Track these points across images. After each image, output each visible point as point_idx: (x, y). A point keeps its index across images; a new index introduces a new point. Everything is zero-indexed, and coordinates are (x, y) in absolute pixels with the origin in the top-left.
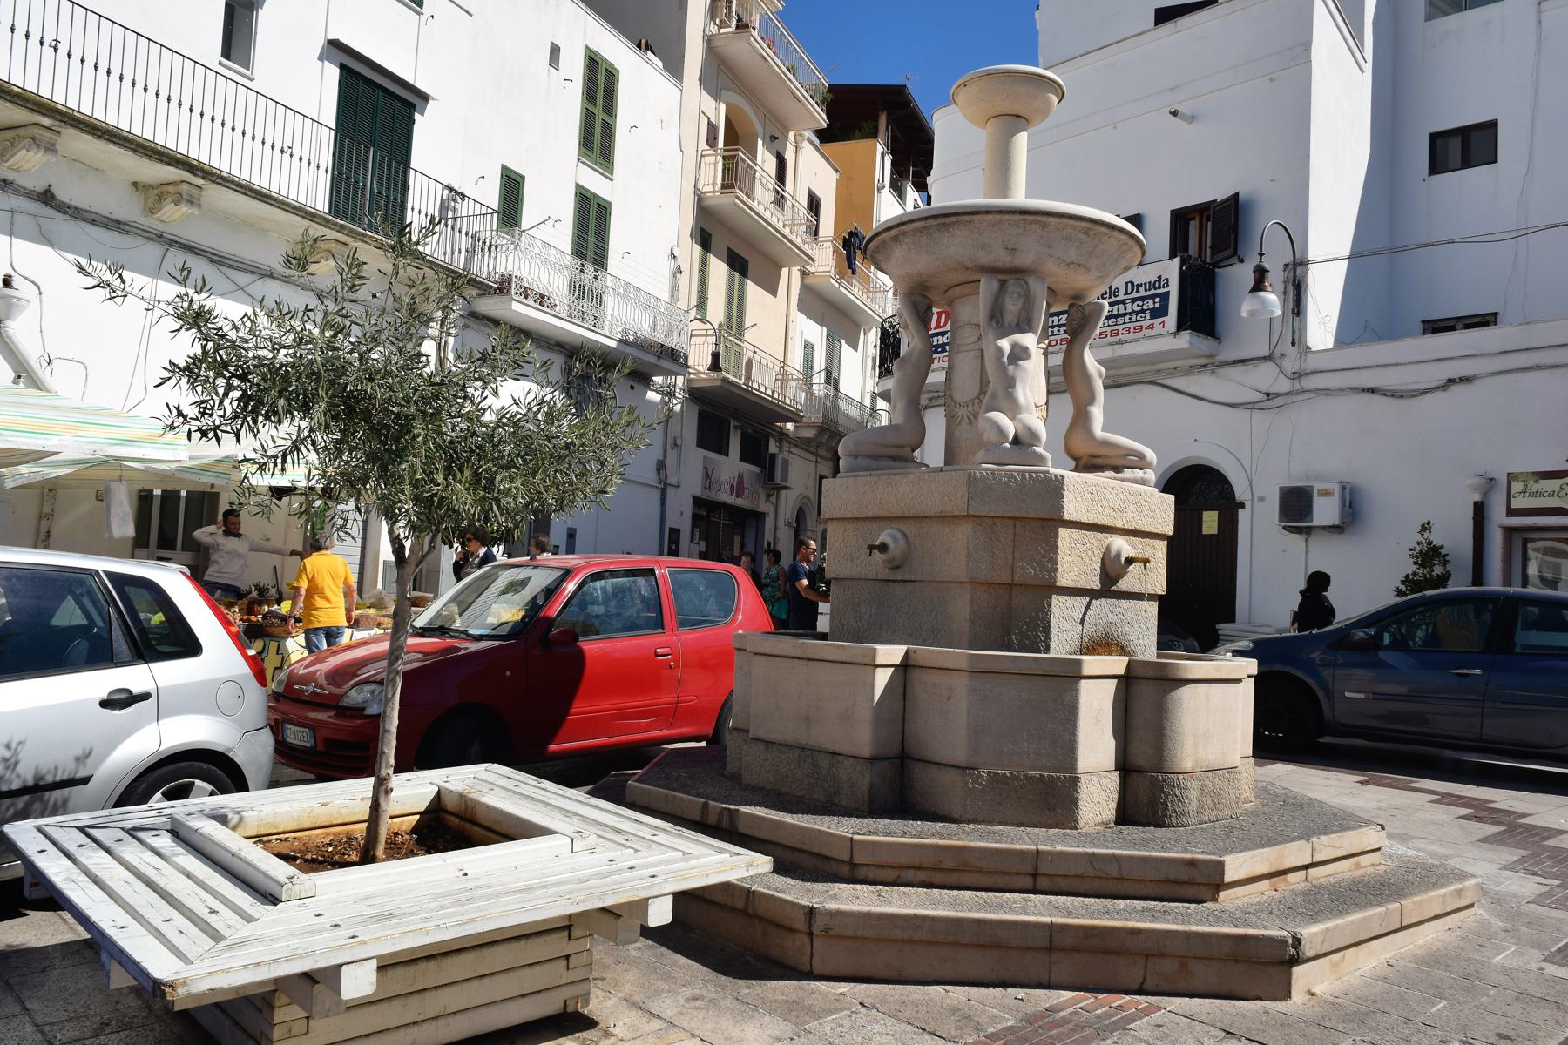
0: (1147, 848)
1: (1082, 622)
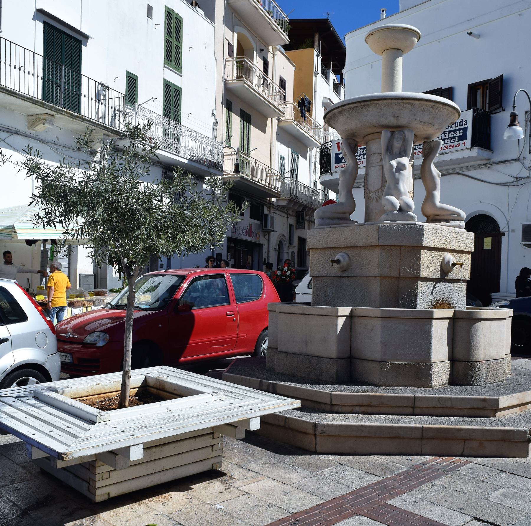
0: (464, 394)
1: (432, 293)
